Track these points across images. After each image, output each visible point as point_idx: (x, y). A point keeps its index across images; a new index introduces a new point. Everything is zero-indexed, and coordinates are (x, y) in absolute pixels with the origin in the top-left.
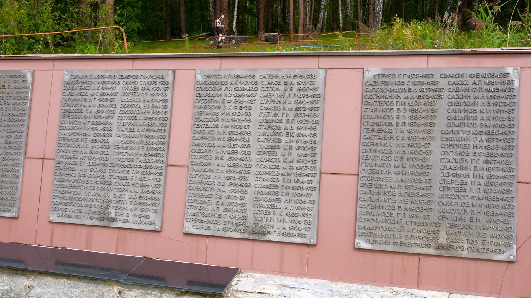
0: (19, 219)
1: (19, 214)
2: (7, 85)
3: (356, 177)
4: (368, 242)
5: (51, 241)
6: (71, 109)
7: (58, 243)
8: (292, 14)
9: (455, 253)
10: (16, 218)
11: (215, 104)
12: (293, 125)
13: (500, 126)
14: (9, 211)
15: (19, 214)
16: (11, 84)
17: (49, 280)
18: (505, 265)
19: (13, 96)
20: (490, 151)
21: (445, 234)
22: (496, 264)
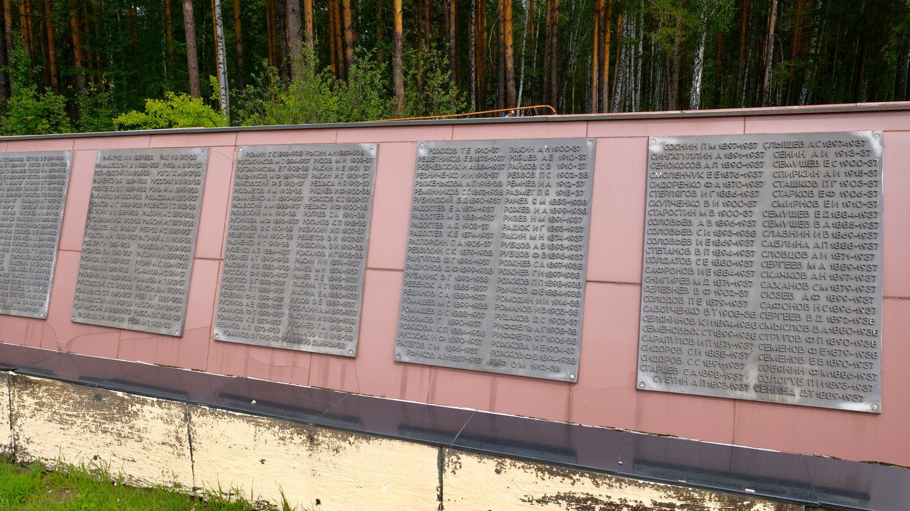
0: (357, 360)
1: (357, 354)
2: (821, 161)
3: (637, 288)
4: (657, 379)
5: (569, 413)
6: (427, 215)
7: (651, 427)
8: (554, 82)
9: (502, 370)
10: (353, 358)
11: (156, 218)
12: (712, 219)
13: (855, 205)
14: (860, 399)
15: (357, 354)
16: (832, 158)
17: (385, 442)
18: (309, 356)
19: (838, 180)
20: (841, 241)
21: (757, 370)
22: (791, 410)
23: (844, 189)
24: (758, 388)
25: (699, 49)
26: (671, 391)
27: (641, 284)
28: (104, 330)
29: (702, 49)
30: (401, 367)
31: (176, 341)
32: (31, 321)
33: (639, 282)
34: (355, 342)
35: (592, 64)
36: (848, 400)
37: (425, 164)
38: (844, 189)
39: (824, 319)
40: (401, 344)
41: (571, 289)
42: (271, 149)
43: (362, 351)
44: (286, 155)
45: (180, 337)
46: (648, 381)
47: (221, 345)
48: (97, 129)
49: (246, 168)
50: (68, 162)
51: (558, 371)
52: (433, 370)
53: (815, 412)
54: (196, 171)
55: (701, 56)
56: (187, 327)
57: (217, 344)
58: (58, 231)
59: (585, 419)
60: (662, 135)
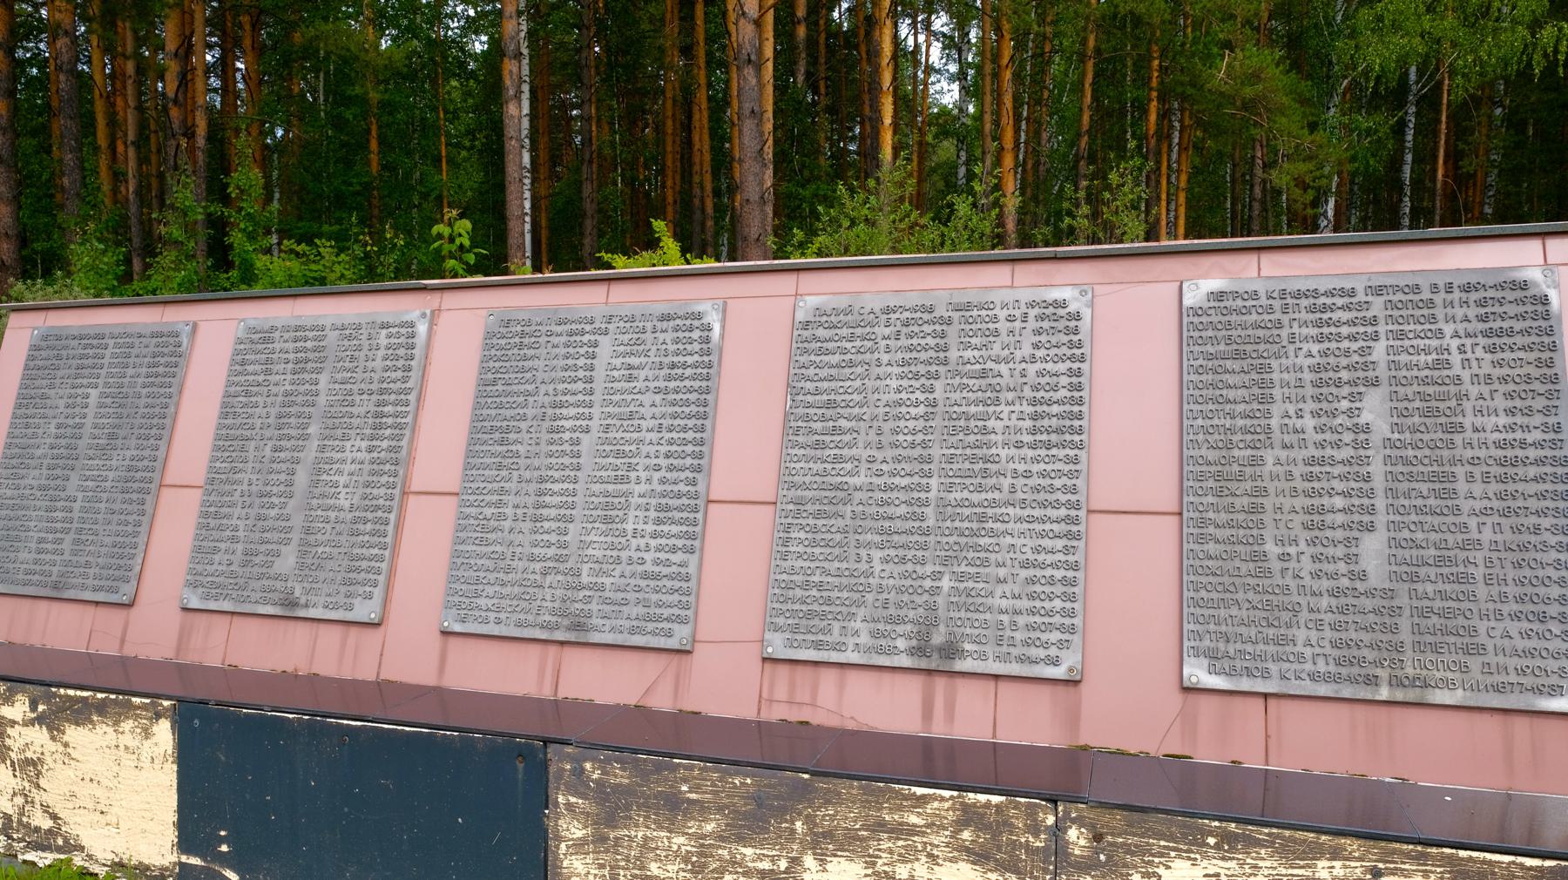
3: (1176, 519)
23: (1510, 404)
24: (912, 652)
25: (1327, 202)
27: (1180, 514)
29: (1331, 204)
32: (354, 630)
33: (1176, 509)
35: (1484, 862)
36: (1541, 693)
38: (1510, 404)
39: (1506, 528)
40: (193, 585)
41: (699, 371)
46: (1198, 673)
50: (185, 341)
54: (406, 351)
55: (1330, 213)
58: (157, 465)
59: (1096, 734)
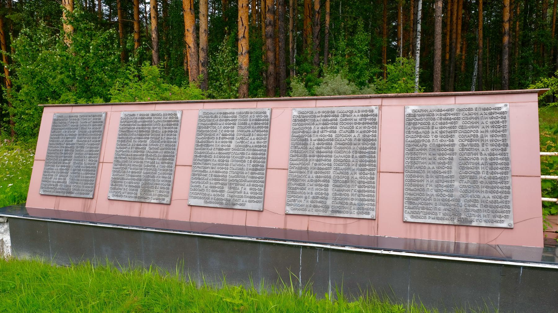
6: (300, 142)
18: (245, 211)
26: (334, 216)
28: (503, 230)
30: (190, 207)
31: (166, 207)
34: (169, 197)
37: (301, 119)
42: (216, 111)
43: (266, 207)
44: (488, 109)
45: (169, 204)
47: (408, 225)
48: (237, 98)
49: (57, 123)
51: (502, 222)
52: (457, 227)
53: (206, 208)
54: (174, 123)
56: (173, 198)
57: (404, 224)
60: (413, 106)
